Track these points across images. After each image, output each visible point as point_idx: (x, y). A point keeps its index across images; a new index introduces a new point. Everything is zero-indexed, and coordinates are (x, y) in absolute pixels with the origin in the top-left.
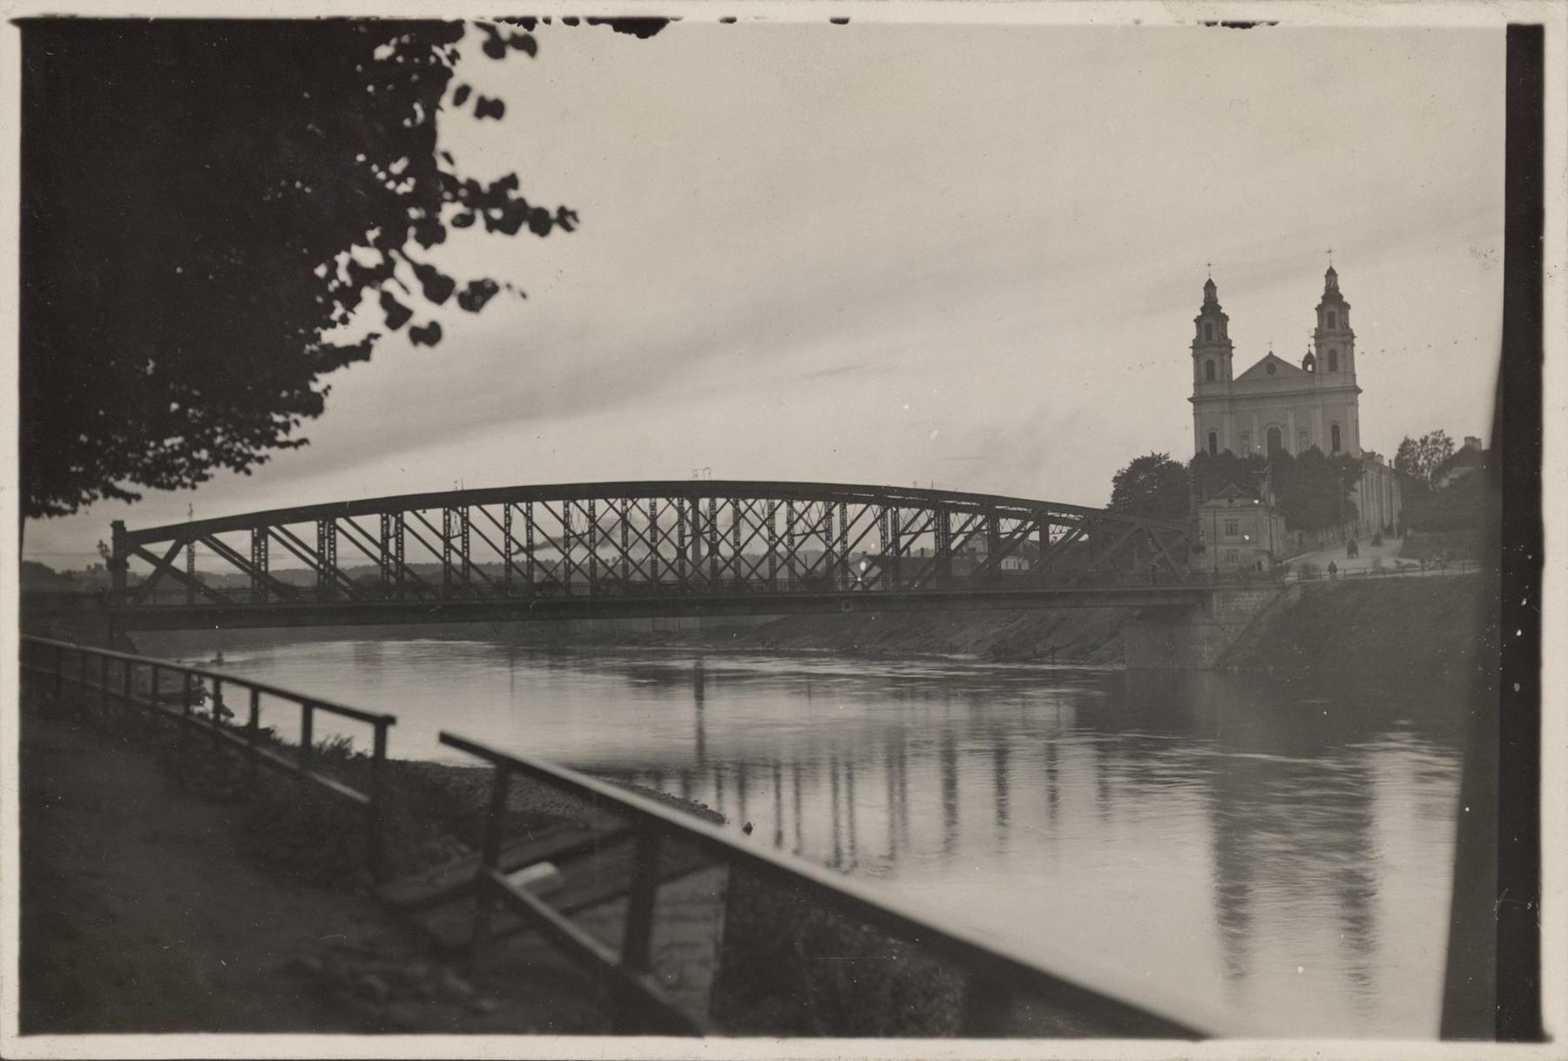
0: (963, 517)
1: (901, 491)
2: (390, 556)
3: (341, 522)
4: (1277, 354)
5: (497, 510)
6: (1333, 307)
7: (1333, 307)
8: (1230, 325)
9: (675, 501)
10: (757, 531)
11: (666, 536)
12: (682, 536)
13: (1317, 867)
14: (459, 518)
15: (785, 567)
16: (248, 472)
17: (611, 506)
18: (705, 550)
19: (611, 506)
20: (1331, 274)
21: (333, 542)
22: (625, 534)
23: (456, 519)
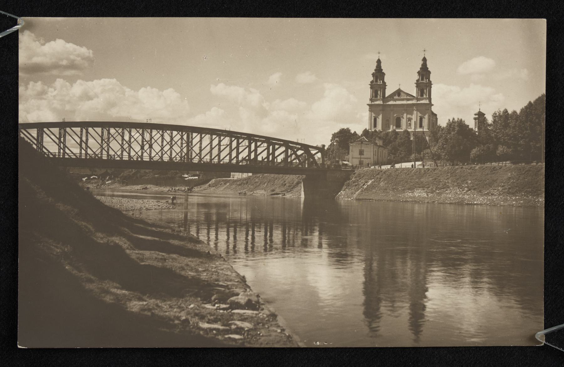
0: (35, 135)
1: (225, 131)
2: (61, 142)
3: (45, 129)
4: (401, 89)
5: (99, 130)
6: (424, 72)
7: (424, 72)
8: (431, 75)
9: (180, 133)
10: (176, 143)
11: (156, 141)
12: (182, 144)
13: (255, 290)
14: (107, 132)
15: (197, 157)
16: (475, 115)
17: (117, 131)
18: (167, 148)
19: (117, 131)
20: (425, 60)
21: (42, 138)
22: (162, 142)
23: (106, 132)
